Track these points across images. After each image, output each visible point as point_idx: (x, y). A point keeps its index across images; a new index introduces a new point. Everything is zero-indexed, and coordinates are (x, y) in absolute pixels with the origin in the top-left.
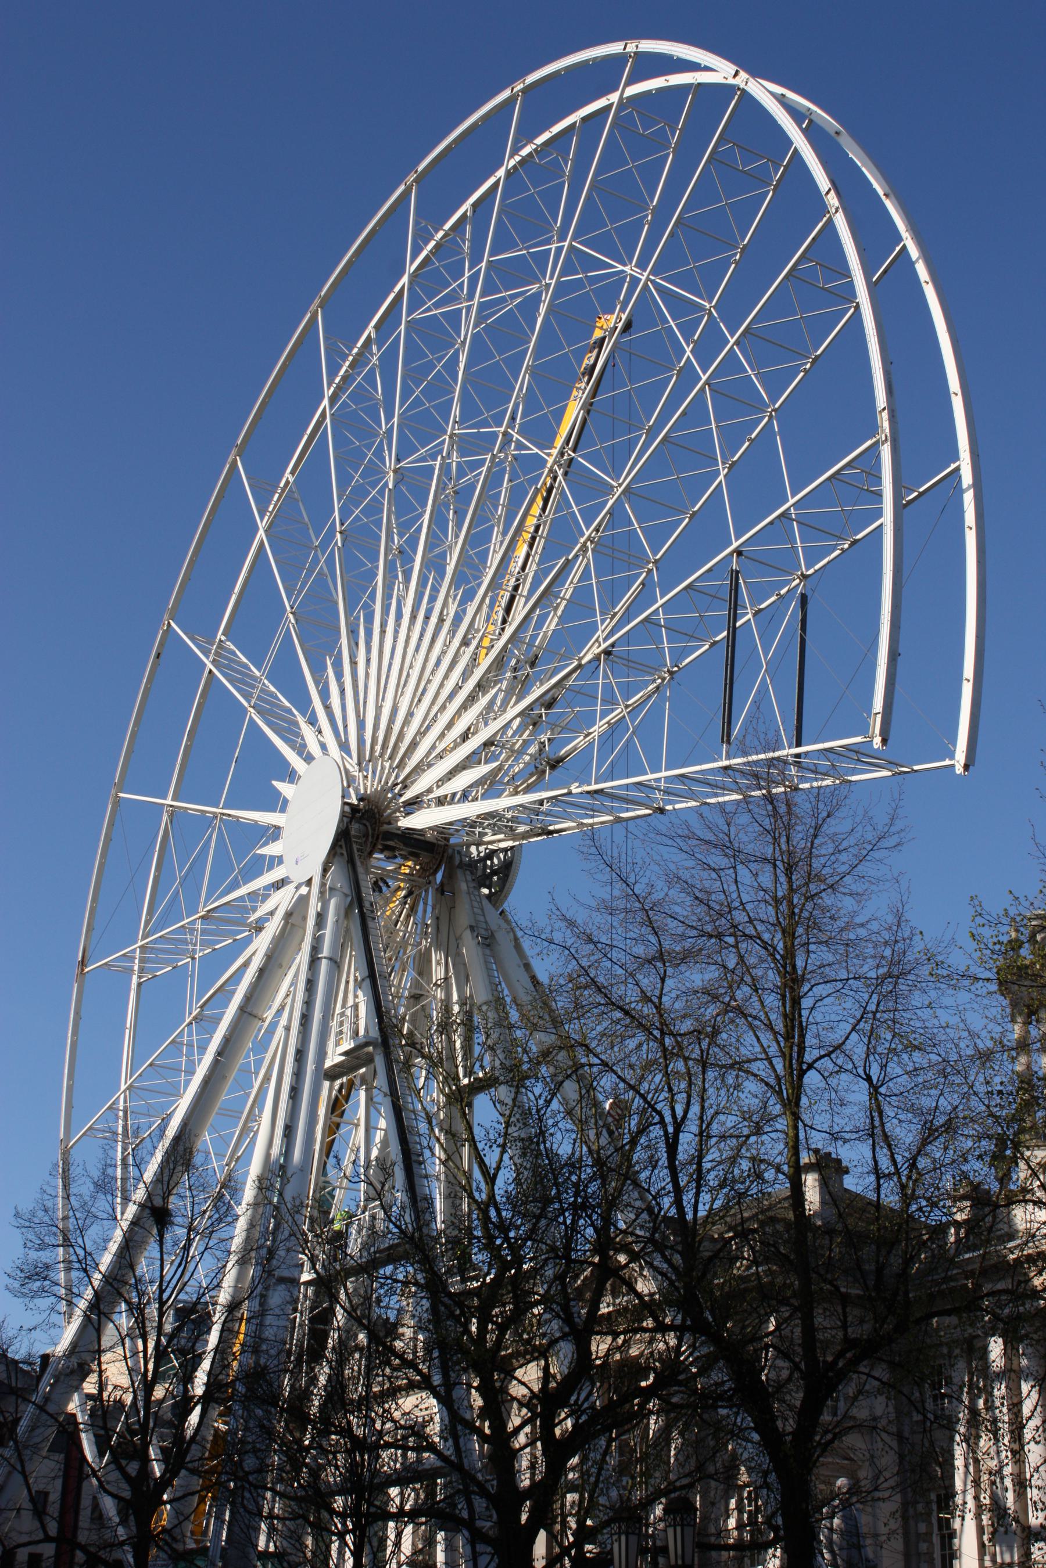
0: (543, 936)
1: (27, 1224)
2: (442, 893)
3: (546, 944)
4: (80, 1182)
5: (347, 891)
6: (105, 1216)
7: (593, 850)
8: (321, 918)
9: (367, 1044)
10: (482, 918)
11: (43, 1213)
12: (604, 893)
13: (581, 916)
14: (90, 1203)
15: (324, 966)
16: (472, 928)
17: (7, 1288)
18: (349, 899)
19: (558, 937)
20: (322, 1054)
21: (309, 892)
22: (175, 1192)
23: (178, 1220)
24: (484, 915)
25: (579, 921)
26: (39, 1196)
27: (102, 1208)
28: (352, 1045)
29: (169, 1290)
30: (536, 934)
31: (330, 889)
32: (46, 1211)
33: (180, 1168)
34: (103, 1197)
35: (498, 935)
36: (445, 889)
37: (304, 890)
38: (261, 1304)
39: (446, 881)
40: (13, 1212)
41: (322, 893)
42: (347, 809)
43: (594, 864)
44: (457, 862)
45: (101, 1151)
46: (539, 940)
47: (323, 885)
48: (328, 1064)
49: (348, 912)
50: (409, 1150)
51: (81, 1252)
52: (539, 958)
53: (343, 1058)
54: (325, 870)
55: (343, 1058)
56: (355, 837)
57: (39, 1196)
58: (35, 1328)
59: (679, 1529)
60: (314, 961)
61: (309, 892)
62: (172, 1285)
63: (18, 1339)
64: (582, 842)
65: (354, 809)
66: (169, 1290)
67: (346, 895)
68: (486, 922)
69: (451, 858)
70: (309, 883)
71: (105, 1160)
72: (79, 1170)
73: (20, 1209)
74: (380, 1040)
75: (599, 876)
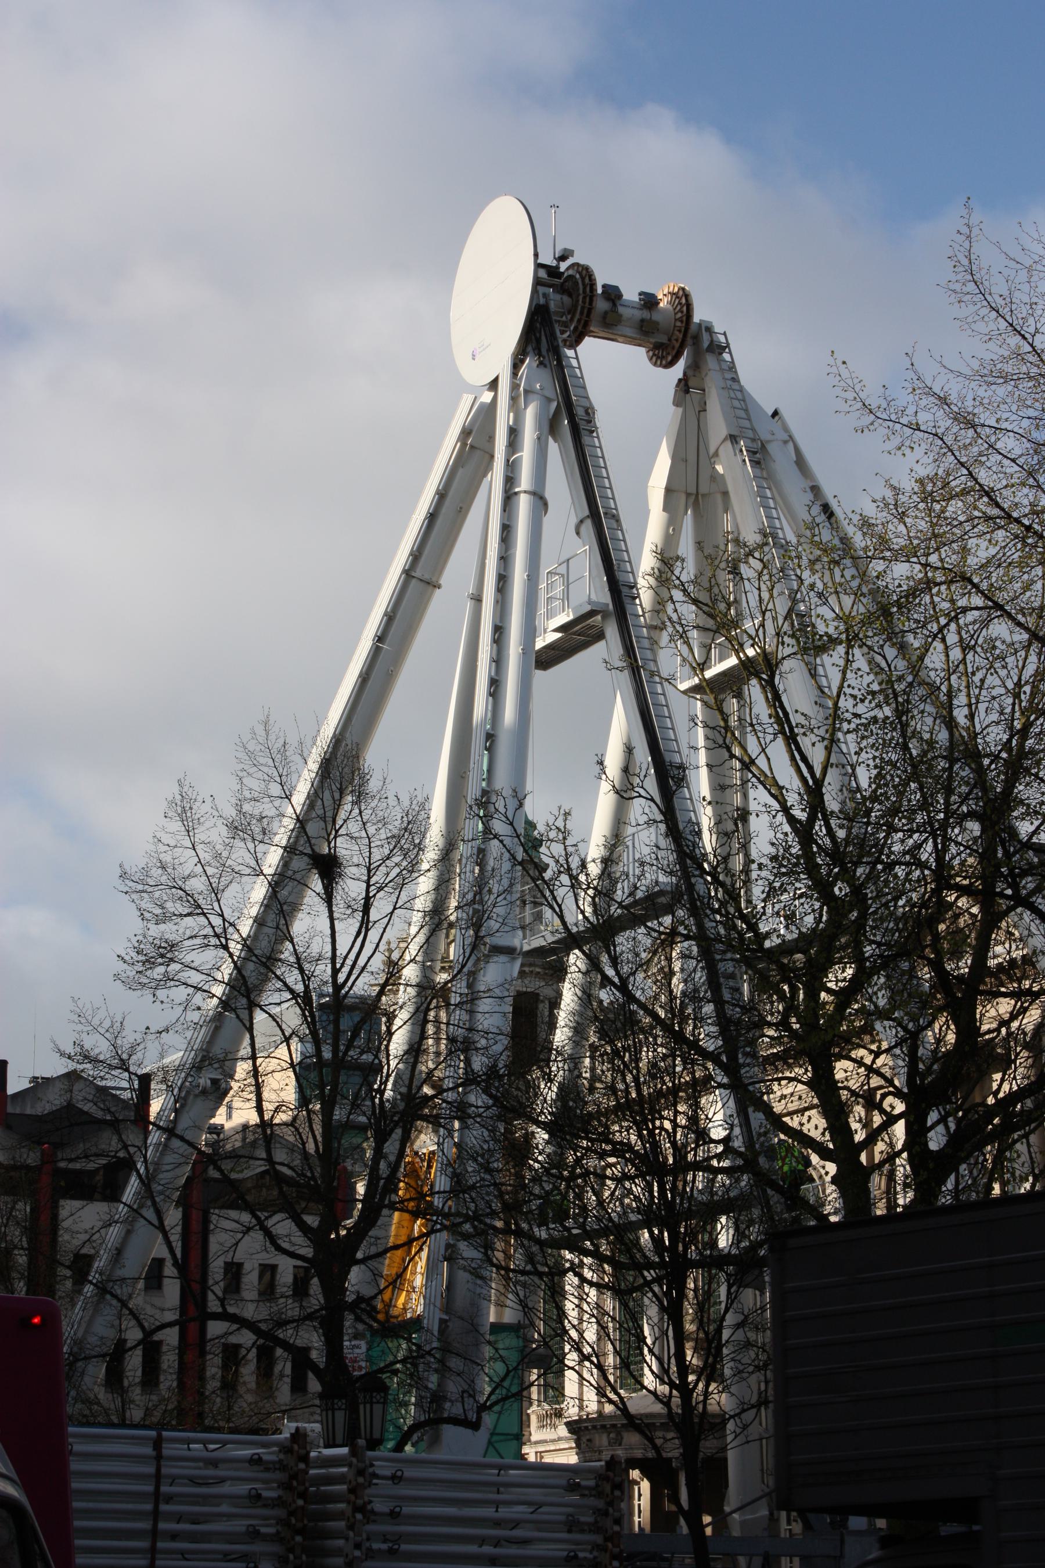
0: (904, 421)
1: (140, 887)
2: (687, 392)
3: (908, 431)
4: (208, 824)
5: (550, 393)
6: (248, 871)
7: (971, 287)
8: (514, 433)
9: (592, 613)
10: (746, 424)
11: (160, 871)
12: (994, 351)
13: (954, 389)
14: (225, 854)
15: (524, 504)
16: (733, 439)
17: (117, 977)
18: (554, 405)
19: (924, 418)
20: (530, 631)
21: (495, 399)
22: (342, 831)
23: (351, 871)
24: (749, 420)
25: (953, 398)
26: (153, 848)
27: (240, 861)
28: (571, 617)
29: (346, 969)
30: (893, 417)
31: (526, 391)
32: (163, 868)
33: (349, 798)
34: (242, 844)
35: (771, 448)
36: (690, 384)
37: (487, 397)
38: (470, 986)
39: (690, 373)
40: (119, 872)
41: (514, 399)
42: (542, 274)
43: (972, 309)
44: (706, 344)
45: (234, 778)
46: (898, 426)
47: (514, 387)
48: (539, 644)
49: (551, 427)
50: (663, 761)
51: (217, 921)
52: (899, 453)
53: (559, 635)
54: (516, 366)
55: (559, 635)
56: (556, 313)
57: (153, 848)
58: (167, 1030)
59: (330, 1413)
60: (509, 498)
61: (495, 399)
62: (349, 962)
63: (142, 1046)
64: (954, 278)
65: (553, 272)
66: (346, 969)
67: (549, 400)
68: (753, 429)
69: (697, 339)
70: (494, 385)
71: (240, 791)
72: (206, 807)
73: (127, 868)
74: (611, 607)
75: (981, 327)
